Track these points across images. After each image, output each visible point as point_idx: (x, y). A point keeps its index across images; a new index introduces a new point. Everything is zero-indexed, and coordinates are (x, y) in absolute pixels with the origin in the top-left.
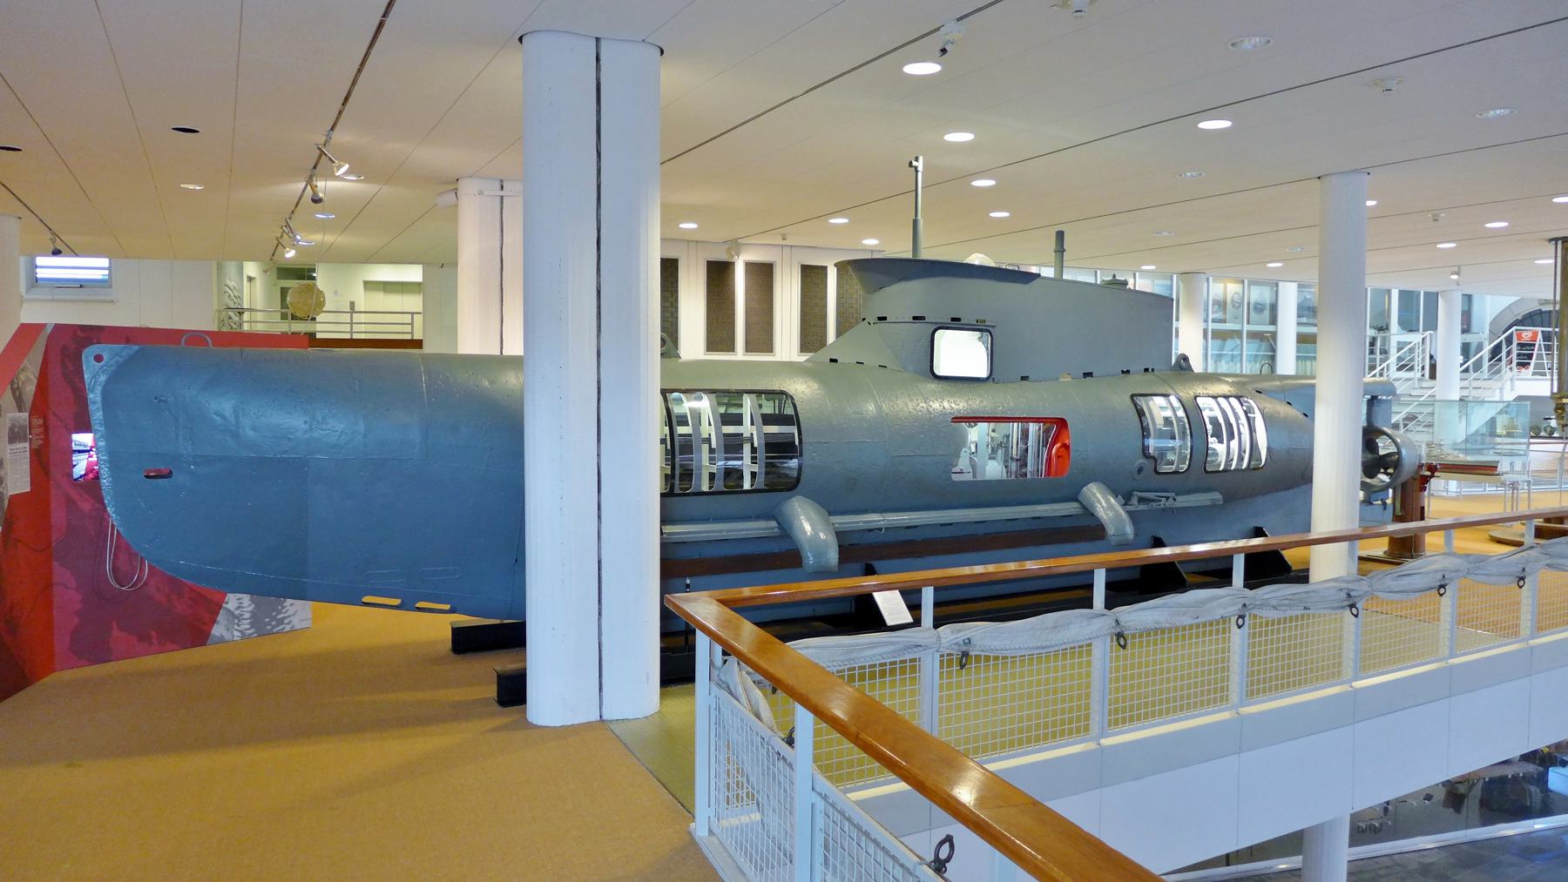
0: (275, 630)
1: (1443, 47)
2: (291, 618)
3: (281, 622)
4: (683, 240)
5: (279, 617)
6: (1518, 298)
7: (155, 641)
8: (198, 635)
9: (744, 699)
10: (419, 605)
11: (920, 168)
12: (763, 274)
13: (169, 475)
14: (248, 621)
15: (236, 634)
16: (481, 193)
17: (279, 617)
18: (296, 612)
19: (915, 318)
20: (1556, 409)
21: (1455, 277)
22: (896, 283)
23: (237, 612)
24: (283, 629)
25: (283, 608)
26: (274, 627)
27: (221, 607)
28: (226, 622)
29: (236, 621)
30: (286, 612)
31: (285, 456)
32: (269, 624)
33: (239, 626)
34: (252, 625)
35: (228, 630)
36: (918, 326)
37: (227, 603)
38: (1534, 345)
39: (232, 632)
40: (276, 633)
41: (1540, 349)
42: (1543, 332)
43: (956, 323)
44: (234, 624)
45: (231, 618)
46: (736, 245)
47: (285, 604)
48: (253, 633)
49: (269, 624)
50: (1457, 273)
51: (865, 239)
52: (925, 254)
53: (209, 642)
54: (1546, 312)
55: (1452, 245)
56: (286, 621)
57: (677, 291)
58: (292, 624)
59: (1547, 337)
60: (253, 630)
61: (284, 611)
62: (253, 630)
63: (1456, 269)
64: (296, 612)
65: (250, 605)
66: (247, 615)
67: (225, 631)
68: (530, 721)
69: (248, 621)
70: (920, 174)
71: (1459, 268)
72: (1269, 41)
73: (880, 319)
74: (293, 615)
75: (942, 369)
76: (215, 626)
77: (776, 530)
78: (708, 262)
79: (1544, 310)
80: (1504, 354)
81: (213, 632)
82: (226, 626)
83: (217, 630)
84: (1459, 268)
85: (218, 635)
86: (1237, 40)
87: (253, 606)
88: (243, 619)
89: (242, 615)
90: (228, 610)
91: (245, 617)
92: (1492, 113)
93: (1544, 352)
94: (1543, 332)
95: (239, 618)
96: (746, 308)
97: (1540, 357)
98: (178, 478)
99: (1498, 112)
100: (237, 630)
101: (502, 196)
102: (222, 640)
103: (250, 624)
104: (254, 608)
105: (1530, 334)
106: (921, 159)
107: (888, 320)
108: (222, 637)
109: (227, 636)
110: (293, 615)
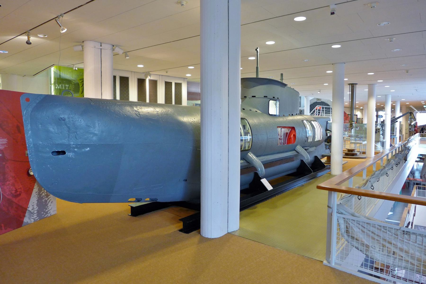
0: (45, 217)
1: (182, 39)
2: (50, 211)
3: (47, 213)
4: (130, 71)
5: (46, 211)
6: (313, 98)
7: (3, 228)
8: (19, 223)
9: (346, 213)
10: (129, 200)
11: (258, 51)
12: (154, 84)
13: (63, 153)
14: (36, 214)
15: (32, 220)
16: (95, 47)
17: (46, 211)
18: (52, 208)
19: (264, 97)
20: (350, 125)
21: (319, 92)
22: (259, 85)
23: (32, 211)
24: (48, 216)
25: (47, 207)
26: (45, 215)
27: (26, 209)
28: (28, 216)
29: (32, 215)
30: (49, 208)
31: (115, 143)
32: (43, 214)
33: (33, 216)
34: (38, 215)
35: (29, 219)
36: (265, 99)
37: (29, 208)
38: (320, 110)
39: (31, 220)
40: (46, 217)
41: (321, 111)
42: (322, 107)
43: (274, 99)
44: (31, 216)
45: (30, 214)
46: (148, 74)
47: (48, 205)
48: (38, 219)
49: (43, 214)
50: (320, 92)
51: (187, 74)
52: (260, 76)
53: (23, 225)
54: (318, 102)
55: (327, 84)
56: (48, 212)
57: (128, 88)
58: (50, 213)
59: (323, 108)
60: (38, 218)
61: (48, 208)
62: (38, 218)
63: (319, 91)
64: (52, 208)
65: (37, 208)
66: (36, 212)
67: (29, 220)
68: (204, 236)
69: (36, 214)
70: (258, 53)
71: (320, 90)
72: (389, 23)
73: (253, 96)
74: (51, 209)
75: (270, 113)
76: (25, 218)
77: (246, 163)
78: (138, 79)
79: (317, 102)
80: (316, 112)
81: (24, 221)
82: (28, 217)
83: (26, 220)
84: (320, 90)
85: (26, 222)
86: (380, 23)
87: (38, 208)
88: (35, 214)
89: (34, 212)
90: (29, 211)
91: (35, 213)
92: (395, 50)
93: (322, 112)
94: (322, 107)
95: (33, 213)
96: (175, 92)
97: (321, 113)
98: (69, 154)
99: (397, 50)
100: (32, 219)
101: (101, 49)
102: (27, 224)
103: (37, 215)
104: (38, 209)
105: (319, 107)
106: (259, 48)
107: (256, 97)
108: (27, 222)
109: (29, 222)
110: (51, 209)
